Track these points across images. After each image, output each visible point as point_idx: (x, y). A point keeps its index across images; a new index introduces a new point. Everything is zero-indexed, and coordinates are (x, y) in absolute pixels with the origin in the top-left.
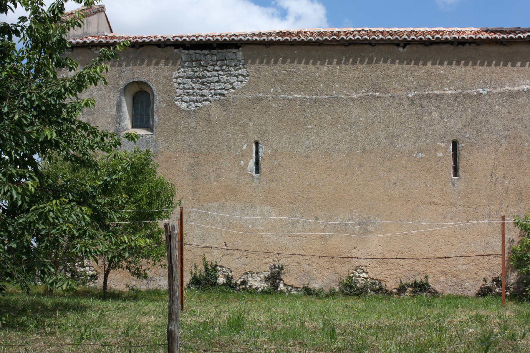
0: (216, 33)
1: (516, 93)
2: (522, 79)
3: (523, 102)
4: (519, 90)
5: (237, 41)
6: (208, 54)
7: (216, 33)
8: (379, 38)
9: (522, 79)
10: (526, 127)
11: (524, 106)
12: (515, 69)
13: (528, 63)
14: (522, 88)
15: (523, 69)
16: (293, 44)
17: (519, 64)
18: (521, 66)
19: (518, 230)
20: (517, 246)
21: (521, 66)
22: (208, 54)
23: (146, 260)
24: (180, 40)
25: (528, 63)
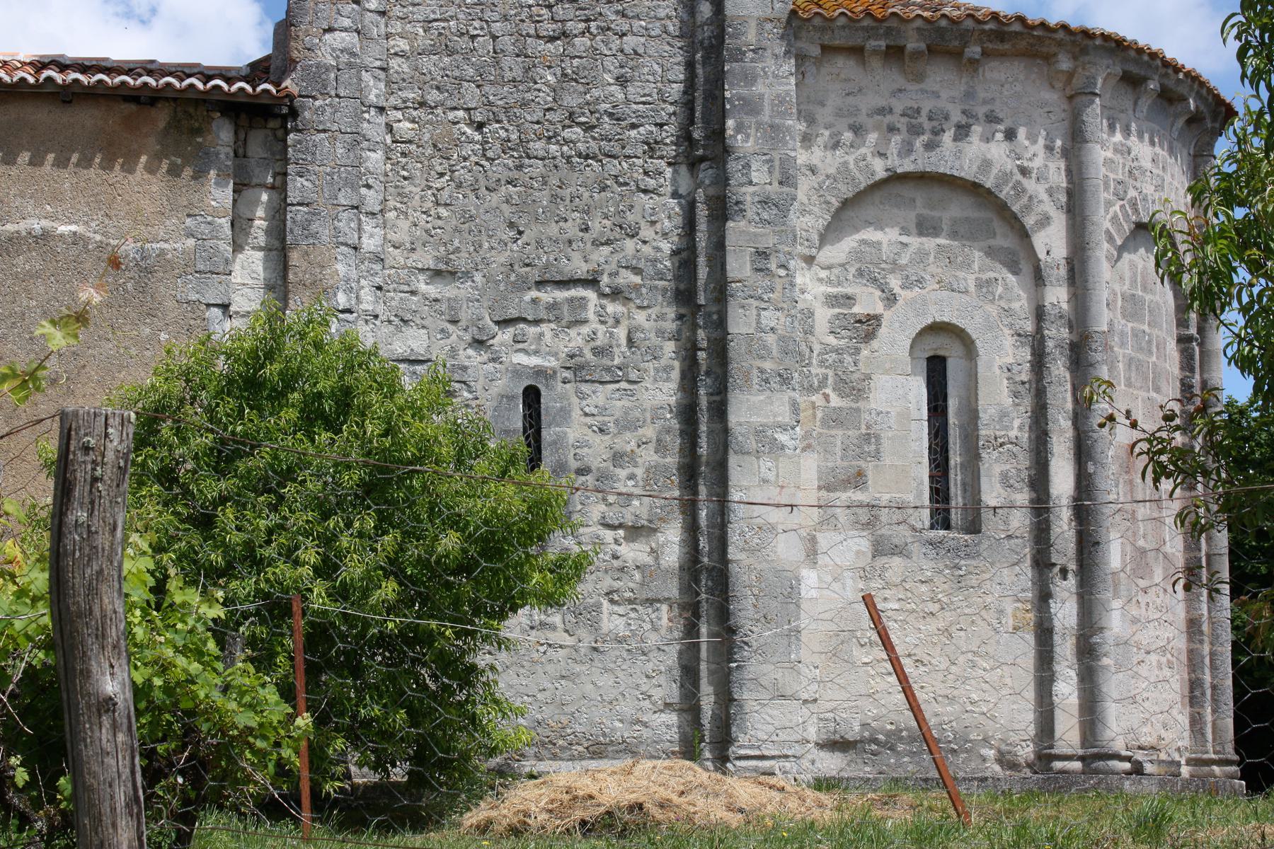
0: (17, 54)
1: (10, 240)
2: (32, 202)
3: (27, 267)
4: (17, 232)
5: (111, 88)
6: (1260, 99)
7: (17, 54)
8: (15, 80)
9: (32, 202)
10: (31, 339)
11: (31, 277)
12: (14, 171)
13: (53, 155)
14: (28, 226)
15: (38, 172)
16: (69, 96)
17: (25, 157)
18: (31, 163)
19: (1143, 260)
20: (1040, 314)
21: (31, 163)
22: (1260, 99)
23: (927, 524)
24: (9, 81)
25: (53, 155)
